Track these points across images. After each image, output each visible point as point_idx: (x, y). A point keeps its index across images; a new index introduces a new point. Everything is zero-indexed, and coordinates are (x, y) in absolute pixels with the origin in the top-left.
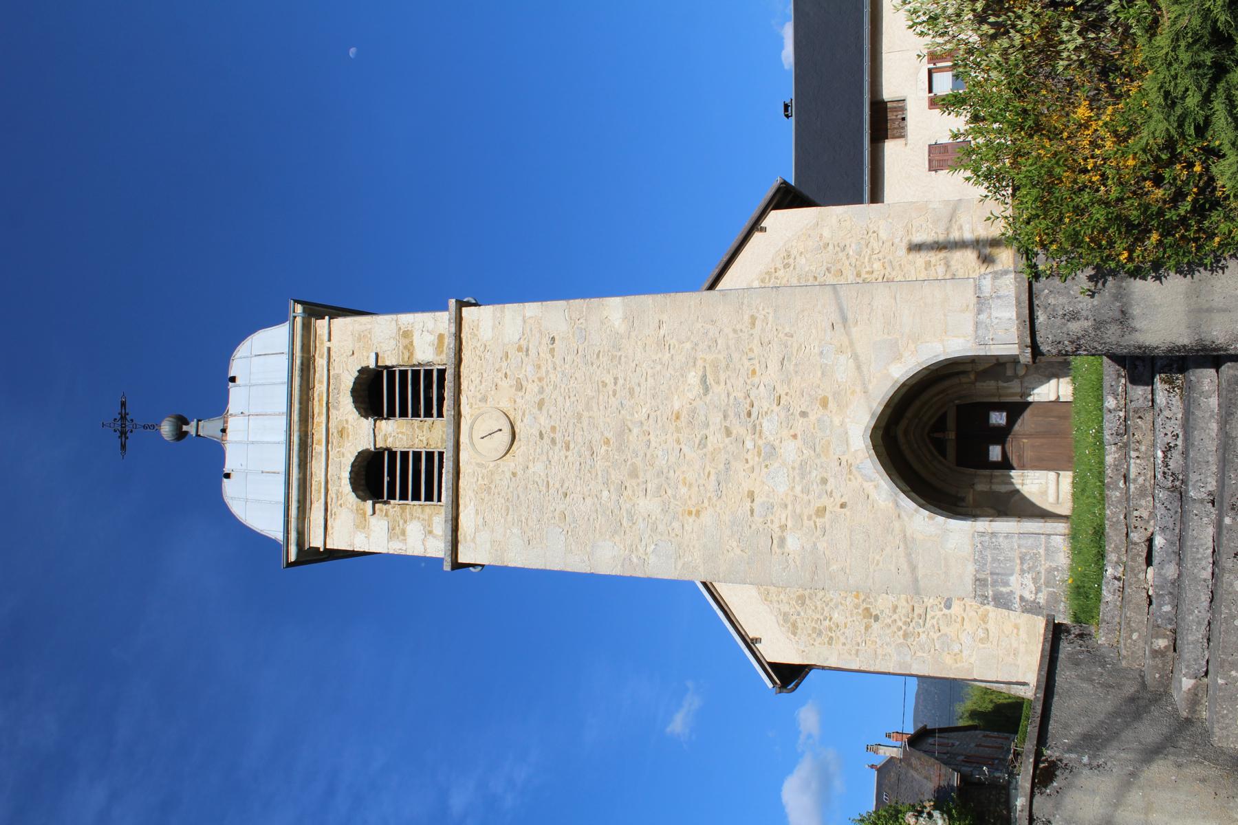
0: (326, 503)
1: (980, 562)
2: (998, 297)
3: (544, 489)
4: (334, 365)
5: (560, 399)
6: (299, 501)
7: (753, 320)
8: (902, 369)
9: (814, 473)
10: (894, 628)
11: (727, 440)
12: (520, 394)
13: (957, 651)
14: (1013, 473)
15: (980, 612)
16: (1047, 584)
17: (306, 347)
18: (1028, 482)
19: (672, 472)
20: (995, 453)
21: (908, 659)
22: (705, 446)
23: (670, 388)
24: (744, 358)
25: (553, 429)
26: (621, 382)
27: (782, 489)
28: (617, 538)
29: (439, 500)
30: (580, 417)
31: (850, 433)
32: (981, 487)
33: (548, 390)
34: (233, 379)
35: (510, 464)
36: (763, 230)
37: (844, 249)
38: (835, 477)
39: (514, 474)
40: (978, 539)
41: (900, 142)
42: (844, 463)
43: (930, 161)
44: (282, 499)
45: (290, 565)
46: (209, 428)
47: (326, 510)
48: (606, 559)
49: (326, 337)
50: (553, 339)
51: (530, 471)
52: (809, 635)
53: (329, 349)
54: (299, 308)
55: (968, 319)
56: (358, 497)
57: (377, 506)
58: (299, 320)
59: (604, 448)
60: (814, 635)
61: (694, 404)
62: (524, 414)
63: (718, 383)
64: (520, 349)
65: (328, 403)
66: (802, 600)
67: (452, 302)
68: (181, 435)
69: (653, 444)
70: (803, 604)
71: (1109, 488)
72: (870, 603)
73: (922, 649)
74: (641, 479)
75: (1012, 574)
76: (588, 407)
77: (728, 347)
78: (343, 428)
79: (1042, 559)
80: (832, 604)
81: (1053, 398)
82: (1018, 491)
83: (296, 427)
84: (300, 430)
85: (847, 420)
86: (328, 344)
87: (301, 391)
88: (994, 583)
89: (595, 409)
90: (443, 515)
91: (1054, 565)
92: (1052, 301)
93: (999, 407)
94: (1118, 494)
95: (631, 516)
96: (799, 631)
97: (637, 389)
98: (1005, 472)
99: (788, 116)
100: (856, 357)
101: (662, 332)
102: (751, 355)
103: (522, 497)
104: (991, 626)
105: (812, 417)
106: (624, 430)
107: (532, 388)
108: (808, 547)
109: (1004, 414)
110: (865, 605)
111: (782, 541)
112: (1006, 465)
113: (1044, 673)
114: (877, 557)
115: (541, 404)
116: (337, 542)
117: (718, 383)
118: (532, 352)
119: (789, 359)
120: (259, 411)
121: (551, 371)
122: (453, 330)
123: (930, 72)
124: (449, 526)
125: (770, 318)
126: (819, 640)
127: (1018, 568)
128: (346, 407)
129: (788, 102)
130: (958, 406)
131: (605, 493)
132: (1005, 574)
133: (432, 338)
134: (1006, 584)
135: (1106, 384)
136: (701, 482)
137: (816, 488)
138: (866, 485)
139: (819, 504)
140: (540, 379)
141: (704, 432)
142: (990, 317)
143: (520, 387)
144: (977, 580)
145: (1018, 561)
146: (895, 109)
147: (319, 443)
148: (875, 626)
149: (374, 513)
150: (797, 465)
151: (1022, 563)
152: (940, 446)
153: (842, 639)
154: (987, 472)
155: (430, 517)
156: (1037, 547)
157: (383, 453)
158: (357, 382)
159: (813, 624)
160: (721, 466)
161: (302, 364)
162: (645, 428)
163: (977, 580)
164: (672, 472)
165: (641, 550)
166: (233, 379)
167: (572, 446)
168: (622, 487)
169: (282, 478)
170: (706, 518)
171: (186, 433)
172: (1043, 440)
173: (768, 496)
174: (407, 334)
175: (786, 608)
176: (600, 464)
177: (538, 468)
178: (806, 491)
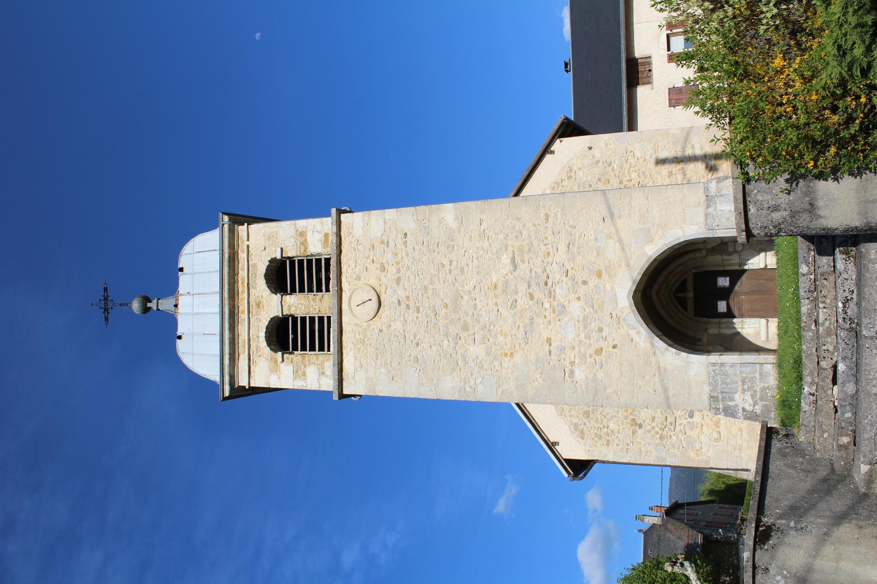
0: (249, 355)
1: (713, 385)
2: (721, 196)
3: (402, 341)
4: (252, 257)
5: (412, 277)
6: (230, 354)
7: (547, 217)
8: (654, 249)
9: (593, 324)
10: (653, 433)
11: (531, 303)
12: (383, 274)
13: (698, 448)
14: (735, 320)
16: (762, 399)
18: (746, 326)
19: (492, 326)
20: (722, 306)
21: (664, 454)
22: (515, 307)
24: (542, 245)
25: (408, 298)
26: (454, 263)
27: (571, 337)
28: (455, 374)
29: (329, 350)
30: (426, 289)
31: (618, 295)
32: (712, 331)
33: (403, 271)
34: (181, 270)
35: (378, 323)
36: (552, 152)
37: (610, 165)
39: (381, 331)
40: (711, 369)
42: (614, 316)
43: (670, 100)
44: (218, 353)
45: (225, 399)
46: (166, 305)
47: (249, 359)
48: (448, 389)
49: (246, 238)
50: (406, 234)
51: (392, 328)
53: (248, 246)
54: (226, 218)
55: (701, 210)
57: (285, 356)
58: (226, 227)
60: (596, 439)
61: (507, 277)
62: (386, 288)
63: (523, 262)
64: (382, 242)
65: (248, 284)
66: (587, 414)
67: (334, 211)
68: (146, 310)
69: (479, 307)
70: (588, 417)
71: (804, 330)
74: (471, 332)
75: (736, 393)
76: (432, 282)
77: (530, 237)
78: (260, 302)
79: (758, 381)
80: (608, 417)
81: (762, 266)
82: (739, 333)
83: (226, 302)
84: (229, 304)
85: (615, 286)
86: (247, 243)
88: (724, 399)
89: (437, 283)
91: (766, 385)
92: (759, 198)
93: (724, 273)
94: (811, 334)
95: (464, 358)
96: (586, 437)
97: (466, 269)
99: (567, 71)
100: (620, 241)
101: (483, 227)
102: (546, 242)
103: (387, 347)
104: (722, 429)
105: (591, 284)
107: (392, 269)
108: (591, 377)
110: (632, 417)
111: (572, 372)
112: (730, 314)
113: (761, 463)
114: (640, 383)
115: (398, 281)
117: (523, 262)
118: (391, 244)
119: (574, 244)
120: (200, 291)
121: (405, 257)
122: (335, 230)
123: (668, 36)
124: (336, 369)
125: (559, 215)
126: (600, 442)
127: (740, 388)
128: (261, 287)
130: (695, 274)
131: (446, 342)
133: (320, 236)
134: (732, 400)
135: (800, 256)
136: (513, 332)
138: (630, 331)
139: (597, 346)
141: (515, 297)
142: (716, 209)
143: (383, 269)
146: (644, 64)
147: (243, 312)
148: (640, 432)
149: (283, 360)
151: (743, 385)
152: (682, 303)
153: (617, 442)
154: (717, 320)
155: (323, 362)
158: (268, 269)
160: (527, 321)
161: (229, 257)
164: (492, 326)
165: (472, 382)
166: (181, 270)
167: (421, 310)
168: (458, 338)
169: (218, 338)
170: (518, 358)
171: (150, 308)
172: (758, 297)
173: (561, 341)
174: (302, 234)
175: (576, 420)
176: (441, 322)
177: (398, 326)
178: (588, 337)
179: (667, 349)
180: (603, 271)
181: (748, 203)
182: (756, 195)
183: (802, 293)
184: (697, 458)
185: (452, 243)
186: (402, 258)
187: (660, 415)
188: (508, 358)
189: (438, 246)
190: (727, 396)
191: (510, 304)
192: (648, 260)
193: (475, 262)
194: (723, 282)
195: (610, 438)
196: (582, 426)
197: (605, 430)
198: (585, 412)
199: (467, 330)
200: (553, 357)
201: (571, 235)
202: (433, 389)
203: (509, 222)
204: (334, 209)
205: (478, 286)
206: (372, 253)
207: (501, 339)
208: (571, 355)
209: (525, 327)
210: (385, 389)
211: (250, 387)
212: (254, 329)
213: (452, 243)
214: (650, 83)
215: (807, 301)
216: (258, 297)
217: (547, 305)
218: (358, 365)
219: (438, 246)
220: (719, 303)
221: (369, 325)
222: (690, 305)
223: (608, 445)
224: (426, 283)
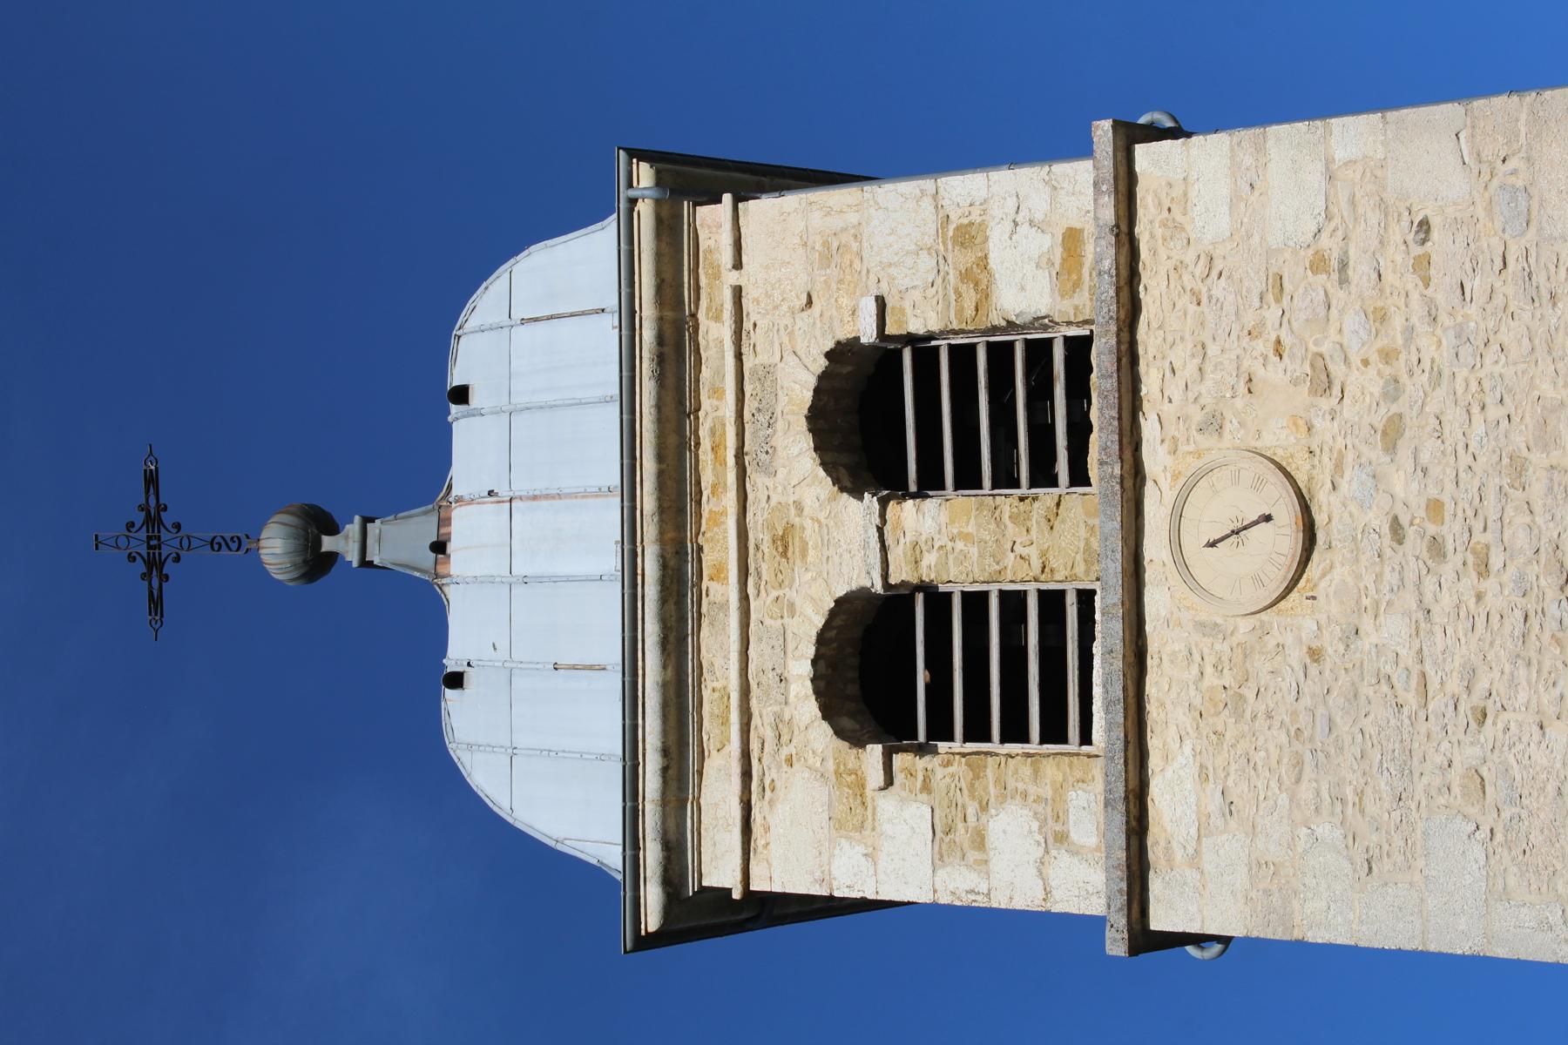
3: (1411, 699)
5: (1454, 416)
6: (665, 752)
12: (1326, 403)
25: (1435, 508)
29: (1086, 738)
30: (1518, 468)
33: (1413, 388)
34: (461, 395)
35: (1299, 622)
39: (1315, 654)
44: (614, 744)
45: (645, 942)
46: (397, 542)
47: (747, 775)
50: (1424, 226)
53: (738, 292)
54: (645, 174)
56: (840, 733)
57: (899, 760)
58: (645, 209)
62: (1339, 467)
64: (1318, 264)
65: (740, 454)
67: (1103, 130)
68: (316, 564)
83: (649, 530)
84: (661, 540)
86: (733, 278)
90: (1099, 786)
103: (1343, 726)
107: (1364, 384)
115: (1391, 434)
116: (784, 871)
118: (1360, 271)
120: (540, 486)
121: (1422, 328)
122: (1108, 215)
124: (1119, 819)
128: (794, 467)
133: (1045, 244)
140: (1387, 356)
143: (1323, 382)
149: (889, 781)
155: (1059, 789)
161: (660, 340)
167: (1496, 561)
169: (613, 683)
171: (333, 557)
174: (968, 236)
177: (1390, 632)
186: (1410, 331)
204: (1107, 124)
211: (747, 893)
212: (767, 648)
218: (1214, 803)
224: (1519, 440)
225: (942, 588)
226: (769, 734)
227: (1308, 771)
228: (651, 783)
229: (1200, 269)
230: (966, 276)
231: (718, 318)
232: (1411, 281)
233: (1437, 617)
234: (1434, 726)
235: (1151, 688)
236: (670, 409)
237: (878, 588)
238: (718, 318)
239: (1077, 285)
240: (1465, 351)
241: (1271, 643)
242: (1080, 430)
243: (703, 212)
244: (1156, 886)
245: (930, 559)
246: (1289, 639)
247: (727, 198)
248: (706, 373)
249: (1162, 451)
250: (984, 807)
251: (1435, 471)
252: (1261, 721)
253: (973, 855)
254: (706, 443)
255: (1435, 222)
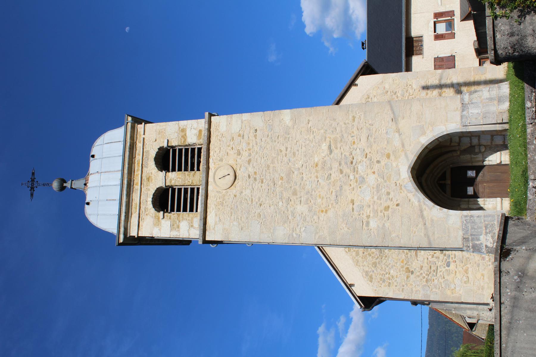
0: (139, 214)
2: (472, 103)
3: (250, 202)
4: (145, 146)
5: (259, 159)
6: (126, 213)
7: (354, 118)
8: (426, 139)
9: (383, 190)
10: (421, 277)
11: (341, 176)
12: (239, 157)
13: (453, 288)
14: (479, 200)
15: (464, 268)
17: (132, 138)
18: (487, 203)
19: (314, 192)
20: (470, 190)
21: (429, 292)
22: (330, 179)
23: (313, 152)
24: (350, 137)
25: (255, 173)
26: (289, 149)
27: (368, 198)
28: (286, 225)
29: (197, 211)
30: (268, 167)
31: (401, 170)
33: (253, 155)
34: (93, 156)
35: (233, 190)
36: (356, 85)
37: (395, 93)
38: (394, 191)
39: (235, 196)
40: (464, 219)
41: (420, 57)
42: (398, 184)
43: (435, 65)
44: (117, 212)
45: (120, 244)
46: (78, 184)
47: (139, 217)
48: (280, 235)
49: (142, 133)
50: (256, 130)
51: (243, 194)
52: (379, 282)
53: (144, 139)
54: (130, 119)
55: (458, 114)
56: (156, 210)
57: (165, 214)
58: (129, 124)
59: (280, 181)
60: (381, 282)
61: (325, 159)
62: (241, 167)
63: (337, 148)
64: (239, 135)
65: (142, 164)
66: (375, 264)
67: (207, 114)
68: (62, 188)
69: (305, 179)
70: (376, 266)
71: (529, 144)
72: (409, 265)
73: (435, 287)
74: (298, 196)
75: (481, 235)
76: (273, 162)
77: (342, 131)
78: (150, 177)
80: (390, 266)
81: (498, 162)
83: (126, 176)
84: (128, 178)
85: (399, 164)
86: (143, 136)
87: (129, 158)
88: (473, 240)
89: (276, 162)
90: (199, 218)
92: (503, 28)
93: (472, 168)
94: (533, 147)
95: (293, 214)
96: (373, 280)
97: (297, 153)
98: (475, 199)
99: (363, 49)
101: (309, 125)
102: (353, 135)
103: (239, 207)
104: (470, 275)
105: (383, 163)
106: (290, 173)
107: (245, 154)
108: (381, 226)
109: (474, 172)
110: (406, 266)
111: (368, 223)
112: (476, 196)
113: (502, 227)
114: (415, 230)
115: (249, 162)
116: (144, 233)
117: (337, 148)
118: (246, 137)
119: (371, 136)
120: (106, 170)
121: (255, 145)
122: (207, 127)
123: (435, 23)
124: (202, 222)
125: (362, 117)
126: (383, 284)
127: (484, 231)
128: (151, 166)
129: (364, 41)
130: (452, 169)
131: (281, 203)
132: (478, 235)
133: (196, 132)
134: (478, 240)
135: (526, 96)
136: (328, 196)
137: (384, 197)
138: (409, 195)
139: (386, 205)
140: (249, 150)
141: (330, 172)
142: (468, 113)
143: (239, 153)
144: (464, 238)
145: (484, 228)
146: (417, 41)
147: (137, 184)
148: (412, 276)
149: (164, 218)
150: (375, 186)
151: (486, 229)
153: (395, 284)
154: (467, 199)
155: (192, 219)
156: (493, 221)
157: (168, 189)
158: (157, 154)
159: (381, 276)
160: (338, 188)
161: (130, 145)
162: (301, 171)
163: (464, 238)
164: (314, 192)
165: (298, 230)
166: (93, 156)
167: (264, 181)
168: (289, 200)
169: (117, 202)
170: (330, 214)
171: (65, 187)
172: (495, 184)
173: (361, 202)
174: (183, 130)
175: (367, 269)
176: (278, 189)
177: (248, 192)
178: (379, 198)
179: (433, 206)
180: (391, 154)
181: (496, 32)
182: (500, 26)
183: (528, 120)
184: (452, 295)
185: (288, 136)
186: (253, 146)
187: (426, 265)
188: (324, 213)
189: (278, 138)
190: (475, 237)
191: (326, 177)
192: (422, 147)
193: (304, 148)
194: (471, 174)
195: (391, 281)
196: (371, 273)
197: (387, 276)
198: (373, 263)
199: (296, 195)
200: (355, 212)
201: (370, 130)
202: (270, 235)
203: (328, 122)
204: (207, 113)
205: (305, 165)
206: (232, 143)
207: (319, 200)
208: (367, 211)
209: (336, 192)
210: (235, 236)
211: (138, 236)
212: (144, 196)
213: (288, 136)
214: (421, 54)
215: (531, 125)
216: (149, 173)
217: (352, 177)
218: (218, 220)
219: (278, 138)
220: (468, 188)
221: (227, 192)
222: (448, 189)
223: (389, 286)
224: (269, 163)
225: (174, 187)
226: (144, 210)
227: (233, 214)
228: (123, 218)
229: (221, 136)
230: (182, 136)
231: (140, 143)
232: (254, 138)
233: (255, 190)
234: (253, 207)
235: (208, 201)
236: (131, 157)
237: (164, 186)
238: (140, 143)
239: (201, 138)
240: (261, 149)
241: (228, 194)
242: (199, 162)
243: (139, 125)
244: (207, 233)
245: (173, 182)
246: (231, 193)
247: (143, 123)
248: (137, 151)
249: (213, 164)
250: (179, 221)
251: (256, 167)
252: (226, 207)
253: (177, 229)
254: (136, 163)
255: (258, 130)
